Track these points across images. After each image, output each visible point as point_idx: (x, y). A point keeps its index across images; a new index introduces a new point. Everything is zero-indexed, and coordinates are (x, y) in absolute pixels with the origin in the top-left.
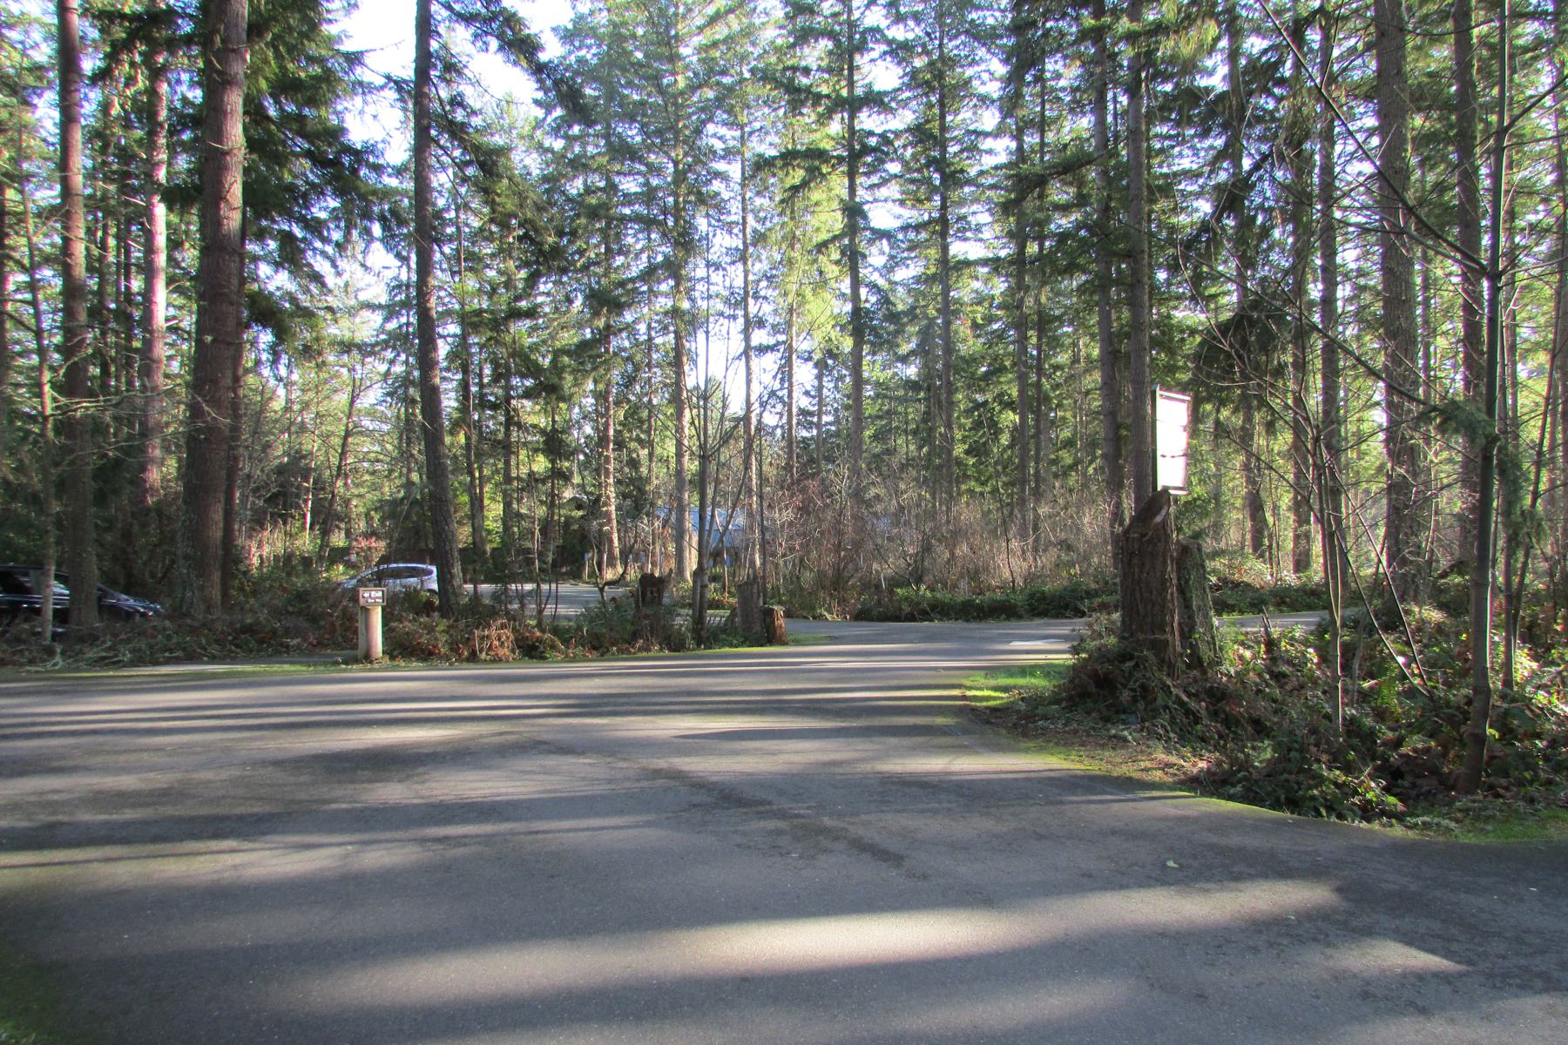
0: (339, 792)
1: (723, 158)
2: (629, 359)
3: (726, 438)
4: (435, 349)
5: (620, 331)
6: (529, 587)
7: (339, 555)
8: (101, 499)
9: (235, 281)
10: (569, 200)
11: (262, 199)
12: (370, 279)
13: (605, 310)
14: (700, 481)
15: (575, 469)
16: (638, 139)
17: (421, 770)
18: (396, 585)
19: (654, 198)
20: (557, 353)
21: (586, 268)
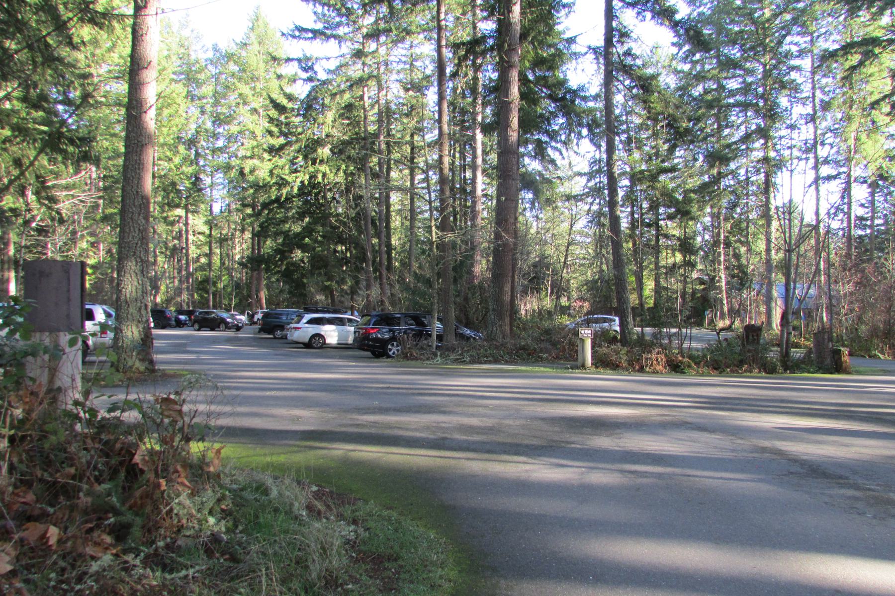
0: (574, 438)
1: (797, 57)
2: (732, 192)
3: (802, 238)
4: (617, 195)
5: (727, 175)
6: (674, 330)
7: (564, 310)
8: (455, 280)
9: (515, 168)
10: (694, 99)
11: (528, 123)
12: (579, 159)
13: (717, 163)
14: (786, 267)
15: (698, 260)
16: (738, 55)
17: (618, 431)
18: (596, 327)
19: (750, 90)
20: (687, 192)
21: (705, 139)
